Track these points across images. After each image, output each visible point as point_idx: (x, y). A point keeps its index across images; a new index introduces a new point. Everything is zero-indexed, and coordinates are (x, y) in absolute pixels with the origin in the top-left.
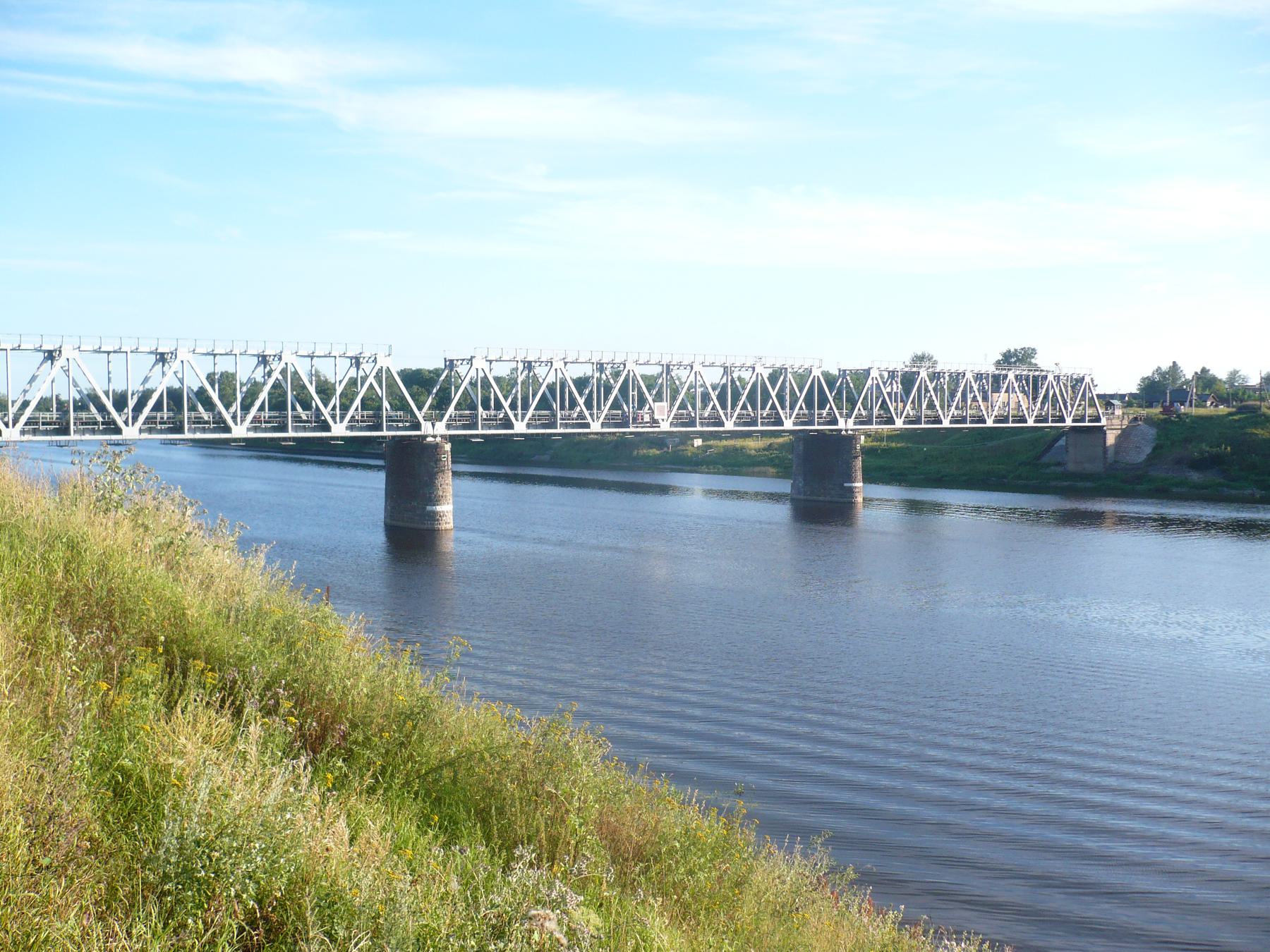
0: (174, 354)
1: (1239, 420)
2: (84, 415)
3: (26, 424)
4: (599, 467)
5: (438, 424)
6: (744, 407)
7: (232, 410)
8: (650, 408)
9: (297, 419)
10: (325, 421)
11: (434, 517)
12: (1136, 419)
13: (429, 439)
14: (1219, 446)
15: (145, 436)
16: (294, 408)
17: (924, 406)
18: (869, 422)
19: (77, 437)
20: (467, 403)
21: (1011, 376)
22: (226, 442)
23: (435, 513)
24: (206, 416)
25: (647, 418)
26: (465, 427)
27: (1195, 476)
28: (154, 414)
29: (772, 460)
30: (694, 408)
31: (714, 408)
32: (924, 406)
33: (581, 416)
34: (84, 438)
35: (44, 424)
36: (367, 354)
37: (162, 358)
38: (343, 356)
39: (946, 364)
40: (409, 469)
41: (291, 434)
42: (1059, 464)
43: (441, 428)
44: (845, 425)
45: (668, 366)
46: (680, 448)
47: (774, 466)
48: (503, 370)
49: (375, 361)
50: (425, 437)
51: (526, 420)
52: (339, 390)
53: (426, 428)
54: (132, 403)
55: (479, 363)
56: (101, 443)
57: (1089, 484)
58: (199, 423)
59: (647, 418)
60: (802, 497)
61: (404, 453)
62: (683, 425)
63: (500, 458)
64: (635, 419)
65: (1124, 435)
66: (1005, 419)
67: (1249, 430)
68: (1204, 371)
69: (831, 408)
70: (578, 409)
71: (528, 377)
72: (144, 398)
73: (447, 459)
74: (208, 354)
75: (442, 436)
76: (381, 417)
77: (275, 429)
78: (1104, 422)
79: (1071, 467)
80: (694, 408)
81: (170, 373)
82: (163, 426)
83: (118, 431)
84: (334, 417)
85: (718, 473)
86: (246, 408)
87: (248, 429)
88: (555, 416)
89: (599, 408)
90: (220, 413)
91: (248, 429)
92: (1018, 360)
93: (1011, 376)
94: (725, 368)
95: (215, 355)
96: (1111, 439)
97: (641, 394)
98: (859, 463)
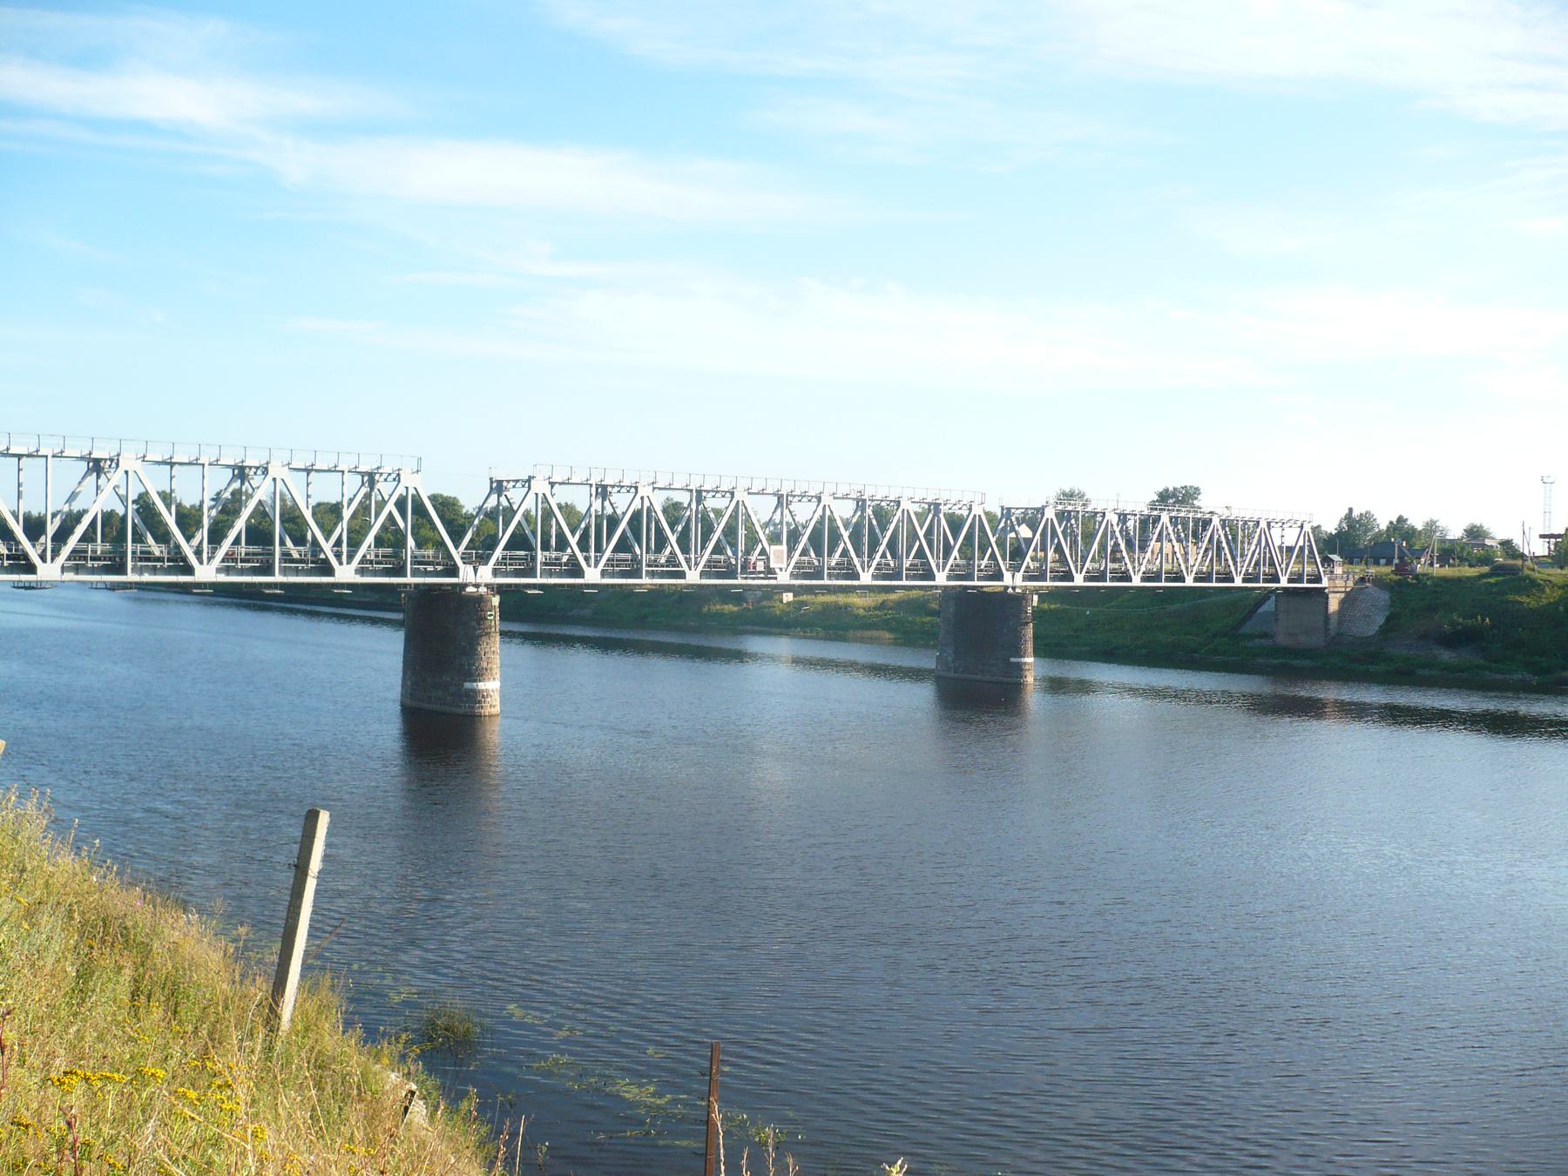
0: (115, 461)
1: (1496, 584)
3: (69, 559)
4: (657, 627)
5: (482, 569)
6: (804, 553)
7: (195, 542)
8: (763, 552)
9: (286, 557)
10: (326, 561)
11: (474, 697)
12: (1362, 580)
13: (470, 589)
14: (1474, 616)
15: (70, 576)
16: (282, 543)
18: (1042, 577)
20: (519, 541)
21: (1165, 518)
22: (185, 589)
23: (476, 692)
24: (156, 549)
26: (517, 573)
27: (1446, 656)
28: (83, 546)
29: (886, 622)
30: (735, 553)
31: (845, 553)
33: (673, 560)
35: (93, 559)
36: (386, 469)
37: (96, 467)
38: (354, 471)
40: (439, 634)
41: (278, 578)
42: (1265, 635)
43: (485, 574)
44: (1013, 581)
45: (699, 492)
46: (765, 603)
47: (891, 630)
48: (327, 490)
49: (398, 479)
51: (601, 566)
52: (347, 514)
53: (466, 574)
54: (51, 529)
55: (540, 486)
56: (94, 587)
57: (1307, 663)
58: (148, 560)
59: (760, 566)
60: (951, 674)
61: (442, 607)
62: (719, 575)
63: (545, 617)
64: (745, 567)
65: (1349, 600)
66: (1156, 577)
67: (1511, 597)
68: (1401, 520)
72: (70, 521)
73: (493, 618)
74: (164, 463)
75: (486, 585)
76: (273, 554)
78: (1325, 583)
79: (1282, 639)
80: (735, 553)
81: (108, 489)
82: (96, 564)
83: (30, 568)
84: (338, 556)
85: (817, 638)
86: (216, 536)
87: (219, 570)
88: (534, 559)
89: (599, 549)
90: (178, 547)
91: (219, 570)
92: (1177, 501)
93: (1165, 518)
94: (780, 497)
95: (172, 464)
96: (1334, 605)
97: (659, 531)
98: (1029, 631)
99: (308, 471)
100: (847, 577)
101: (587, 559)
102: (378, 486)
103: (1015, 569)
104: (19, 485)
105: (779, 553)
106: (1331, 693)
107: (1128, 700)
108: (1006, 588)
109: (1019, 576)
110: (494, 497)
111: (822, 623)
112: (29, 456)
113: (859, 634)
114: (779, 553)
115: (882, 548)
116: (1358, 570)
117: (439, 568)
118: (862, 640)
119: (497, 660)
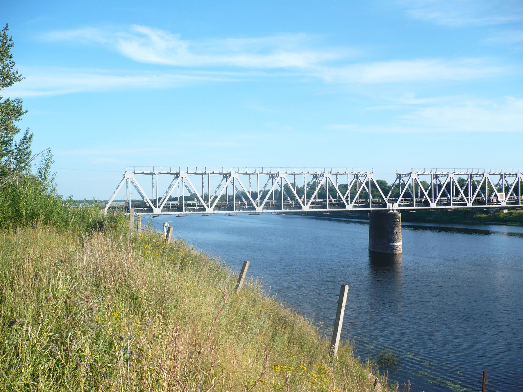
2: (239, 202)
3: (265, 205)
7: (302, 199)
11: (393, 248)
19: (237, 211)
34: (239, 212)
41: (328, 209)
43: (396, 206)
45: (471, 175)
51: (472, 201)
53: (389, 206)
59: (495, 200)
70: (460, 195)
73: (399, 221)
75: (396, 210)
77: (407, 206)
91: (310, 208)
94: (501, 175)
99: (337, 174)
101: (431, 200)
102: (359, 178)
105: (502, 196)
110: (398, 180)
119: (401, 235)
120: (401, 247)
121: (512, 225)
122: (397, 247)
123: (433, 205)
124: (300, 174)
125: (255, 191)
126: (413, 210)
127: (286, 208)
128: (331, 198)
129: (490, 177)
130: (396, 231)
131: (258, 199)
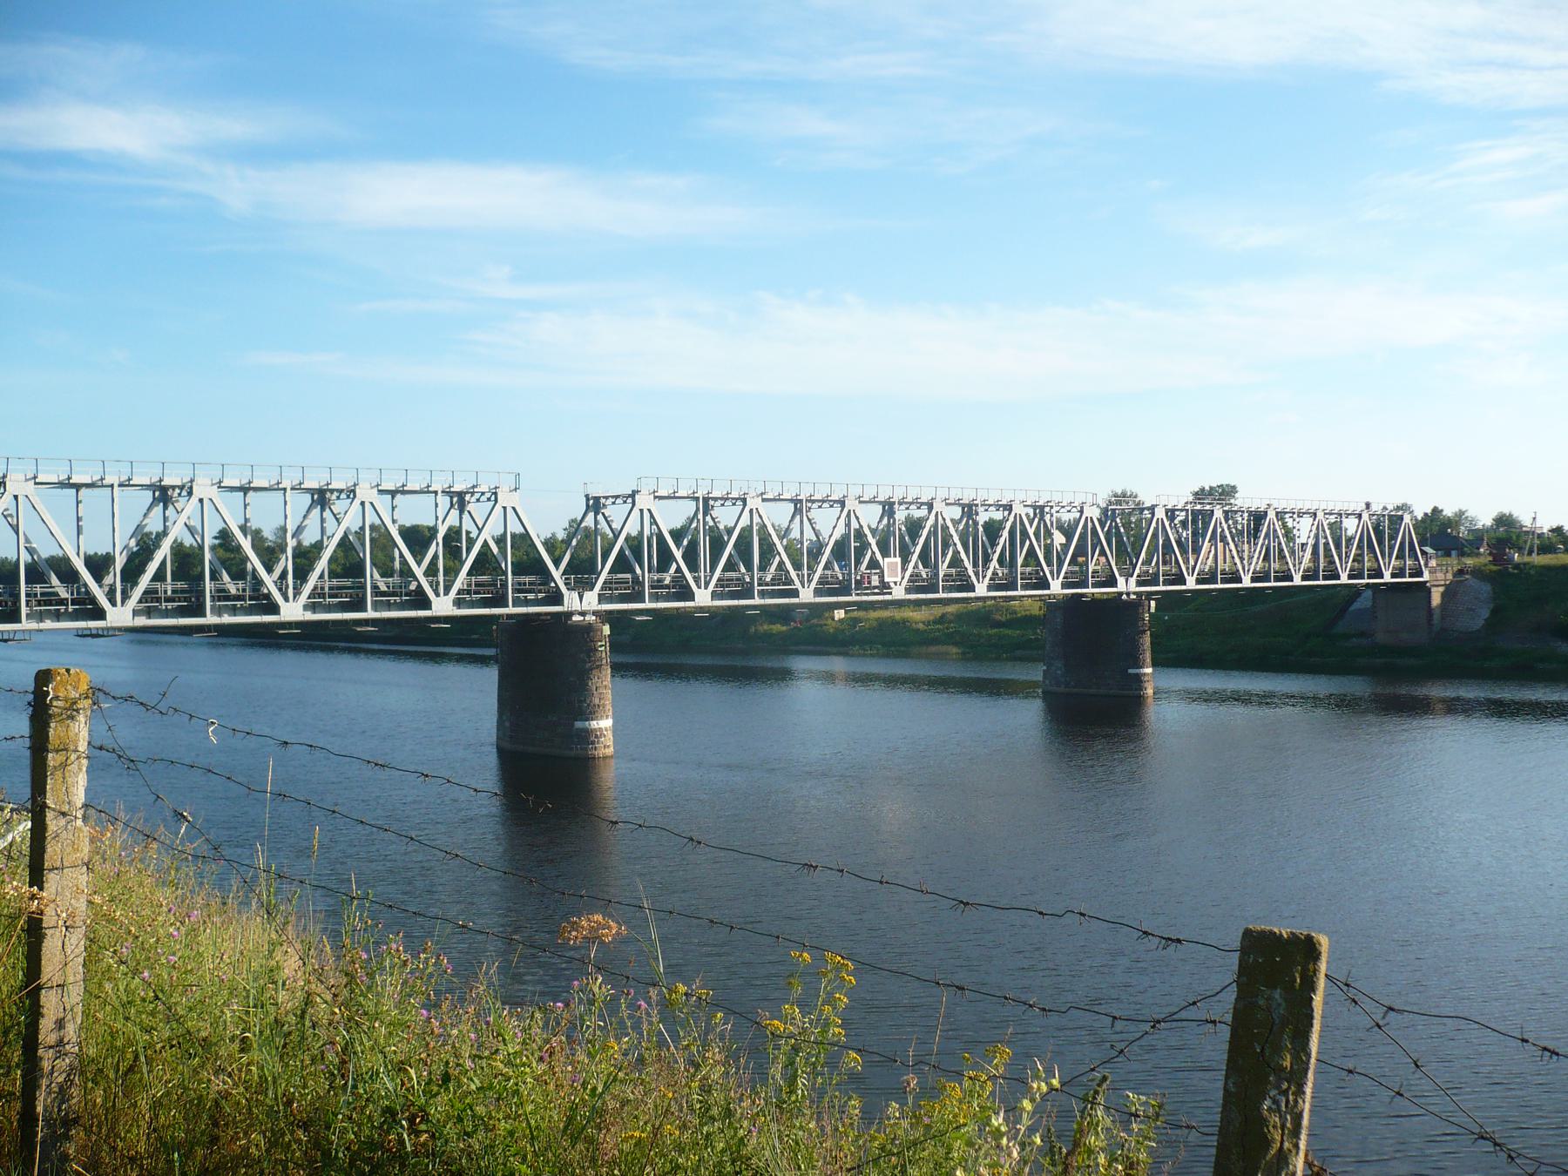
2: (38, 589)
3: (140, 601)
7: (108, 580)
9: (221, 595)
10: (268, 596)
11: (587, 737)
12: (1461, 572)
13: (576, 618)
17: (1020, 561)
19: (34, 625)
25: (875, 581)
30: (749, 567)
32: (1020, 561)
34: (42, 626)
35: (168, 600)
39: (1248, 499)
41: (370, 614)
42: (1362, 634)
43: (591, 600)
44: (1126, 586)
45: (706, 500)
47: (955, 644)
48: (417, 512)
50: (569, 614)
51: (813, 585)
53: (571, 601)
59: (875, 581)
60: (1062, 689)
63: (667, 648)
65: (1450, 593)
66: (1211, 578)
69: (679, 570)
70: (674, 566)
71: (888, 525)
73: (603, 648)
75: (595, 613)
76: (363, 587)
77: (344, 607)
78: (1426, 576)
79: (1381, 638)
80: (749, 567)
82: (170, 605)
87: (306, 608)
91: (306, 608)
94: (796, 502)
96: (1436, 599)
98: (1147, 640)
99: (245, 490)
100: (960, 589)
101: (697, 580)
102: (469, 507)
103: (583, 585)
104: (79, 519)
105: (892, 566)
106: (1438, 691)
107: (1239, 709)
108: (1121, 594)
109: (1133, 580)
110: (591, 515)
111: (882, 644)
112: (88, 486)
113: (924, 649)
114: (892, 566)
115: (915, 557)
116: (1454, 562)
117: (540, 596)
118: (920, 656)
119: (608, 694)
120: (610, 735)
121: (864, 655)
122: (597, 734)
123: (703, 598)
124: (421, 492)
125: (102, 549)
126: (366, 622)
127: (218, 611)
128: (377, 576)
129: (764, 509)
130: (594, 682)
131: (114, 577)
